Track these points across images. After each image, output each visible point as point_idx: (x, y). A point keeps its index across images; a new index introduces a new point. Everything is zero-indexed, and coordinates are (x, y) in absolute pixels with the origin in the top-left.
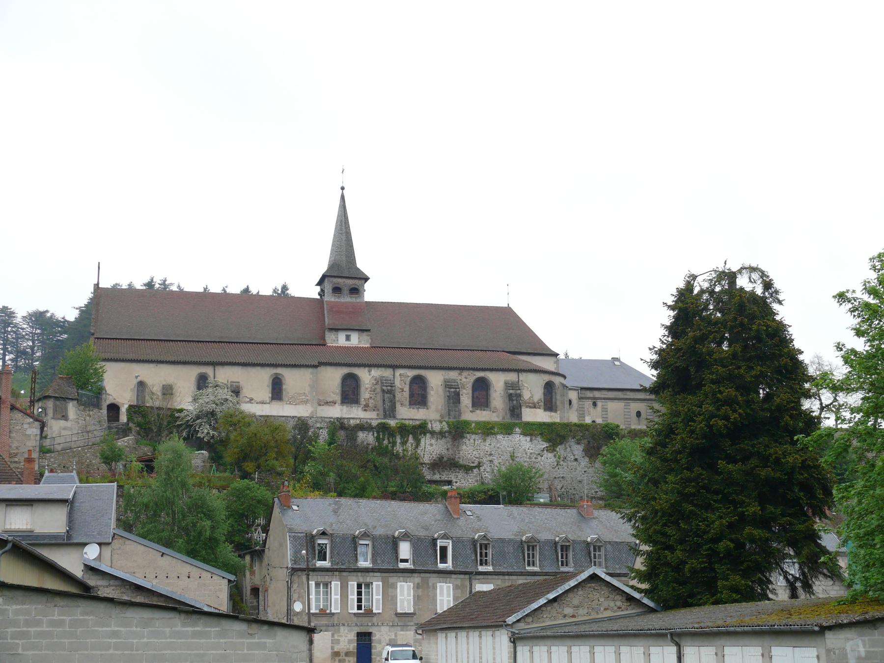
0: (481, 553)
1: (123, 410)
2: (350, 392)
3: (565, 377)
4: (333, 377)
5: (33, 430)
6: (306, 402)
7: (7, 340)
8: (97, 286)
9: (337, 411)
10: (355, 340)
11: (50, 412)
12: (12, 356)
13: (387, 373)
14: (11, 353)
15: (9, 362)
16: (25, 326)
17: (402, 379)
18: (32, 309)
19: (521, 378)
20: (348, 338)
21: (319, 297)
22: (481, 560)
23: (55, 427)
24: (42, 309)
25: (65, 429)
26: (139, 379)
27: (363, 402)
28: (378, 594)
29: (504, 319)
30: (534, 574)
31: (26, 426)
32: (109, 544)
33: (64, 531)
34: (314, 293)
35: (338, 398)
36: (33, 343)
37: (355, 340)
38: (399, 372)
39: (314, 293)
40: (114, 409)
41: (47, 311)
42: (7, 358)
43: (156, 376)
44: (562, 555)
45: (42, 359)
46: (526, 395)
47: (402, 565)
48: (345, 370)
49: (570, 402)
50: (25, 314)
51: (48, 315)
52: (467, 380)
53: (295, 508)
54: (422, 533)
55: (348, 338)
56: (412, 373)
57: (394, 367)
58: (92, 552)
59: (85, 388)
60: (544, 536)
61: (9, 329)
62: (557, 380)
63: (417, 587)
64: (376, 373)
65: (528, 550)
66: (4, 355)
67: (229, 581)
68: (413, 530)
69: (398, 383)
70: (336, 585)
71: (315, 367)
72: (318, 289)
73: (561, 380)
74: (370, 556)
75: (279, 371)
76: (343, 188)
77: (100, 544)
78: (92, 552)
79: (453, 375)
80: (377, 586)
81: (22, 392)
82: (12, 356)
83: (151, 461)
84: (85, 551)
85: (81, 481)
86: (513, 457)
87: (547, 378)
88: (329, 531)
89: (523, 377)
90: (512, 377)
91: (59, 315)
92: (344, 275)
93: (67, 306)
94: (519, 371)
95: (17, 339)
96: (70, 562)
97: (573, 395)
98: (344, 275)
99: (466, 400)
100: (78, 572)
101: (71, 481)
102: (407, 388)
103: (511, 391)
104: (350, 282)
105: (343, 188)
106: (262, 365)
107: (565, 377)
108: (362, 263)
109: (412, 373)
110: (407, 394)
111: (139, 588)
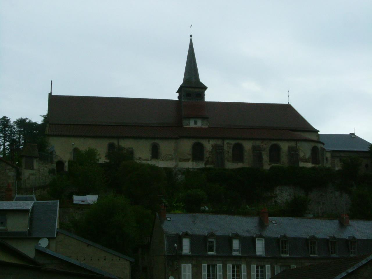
0: (282, 247)
1: (66, 164)
2: (198, 153)
3: (323, 144)
4: (187, 145)
5: (12, 173)
6: (171, 159)
7: (6, 135)
8: (50, 94)
9: (190, 165)
10: (200, 124)
11: (24, 165)
12: (8, 143)
13: (219, 142)
14: (7, 141)
15: (7, 147)
16: (16, 127)
17: (228, 145)
18: (19, 118)
19: (298, 145)
20: (196, 123)
21: (178, 99)
22: (282, 251)
23: (26, 173)
24: (23, 118)
25: (32, 174)
26: (75, 146)
27: (205, 159)
28: (220, 271)
29: (286, 110)
30: (314, 259)
31: (7, 171)
32: (55, 238)
33: (27, 230)
34: (175, 97)
35: (190, 157)
36: (20, 136)
37: (200, 124)
38: (226, 142)
39: (175, 97)
40: (60, 164)
41: (27, 119)
42: (6, 144)
43: (84, 145)
44: (332, 247)
45: (24, 144)
46: (301, 155)
47: (234, 253)
48: (194, 141)
49: (327, 159)
50: (15, 120)
51: (27, 121)
52: (266, 146)
53: (169, 219)
54: (247, 234)
55: (196, 123)
56: (233, 142)
57: (223, 139)
58: (44, 243)
59: (45, 155)
60: (319, 236)
61: (7, 129)
62: (319, 146)
63: (194, 266)
64: (212, 142)
65: (311, 245)
66: (4, 143)
67: (131, 262)
68: (241, 233)
69: (226, 148)
70: (244, 267)
71: (177, 139)
72: (178, 95)
73: (322, 146)
74: (169, 254)
75: (156, 141)
76: (191, 36)
77: (49, 239)
78: (44, 243)
79: (258, 143)
80: (268, 267)
81: (17, 163)
82: (8, 143)
83: (106, 257)
84: (39, 242)
85: (37, 200)
86: (119, 260)
87: (313, 144)
88: (190, 232)
89: (299, 144)
90: (293, 144)
91: (33, 121)
92: (192, 87)
93: (37, 113)
94: (297, 140)
95: (11, 134)
96: (28, 250)
97: (328, 155)
98: (192, 87)
99: (265, 157)
100: (31, 254)
101: (31, 199)
102: (231, 151)
103: (293, 152)
104: (196, 90)
105: (191, 36)
106: (146, 138)
107: (323, 144)
108: (203, 79)
109: (233, 142)
110: (231, 155)
111: (72, 265)
